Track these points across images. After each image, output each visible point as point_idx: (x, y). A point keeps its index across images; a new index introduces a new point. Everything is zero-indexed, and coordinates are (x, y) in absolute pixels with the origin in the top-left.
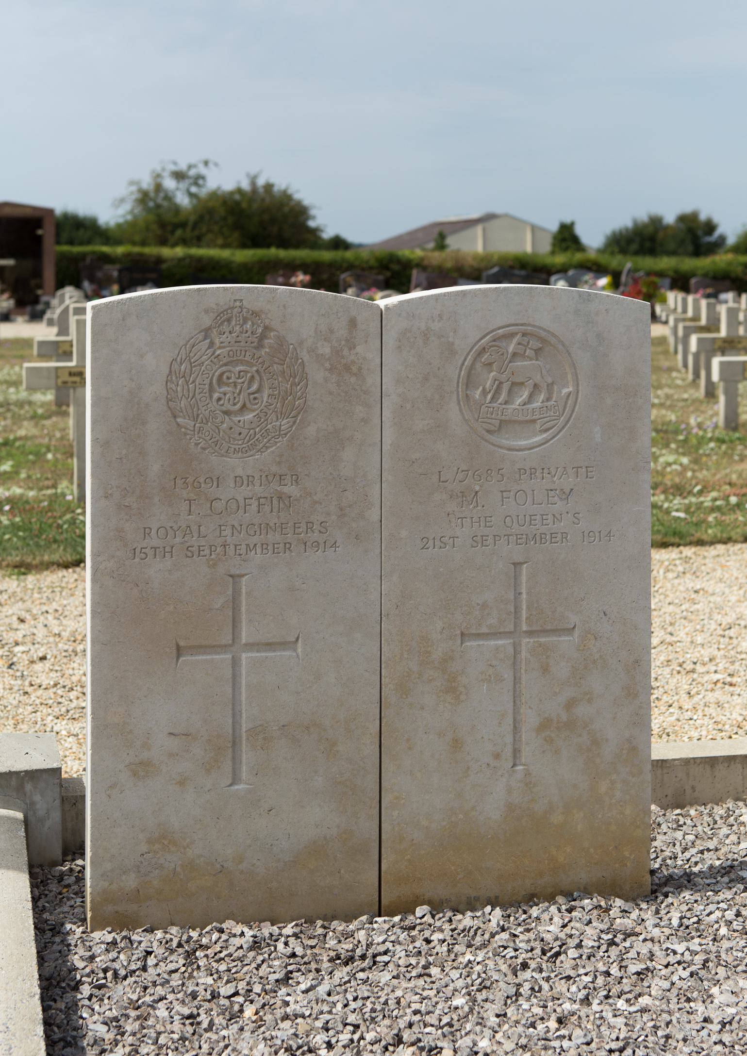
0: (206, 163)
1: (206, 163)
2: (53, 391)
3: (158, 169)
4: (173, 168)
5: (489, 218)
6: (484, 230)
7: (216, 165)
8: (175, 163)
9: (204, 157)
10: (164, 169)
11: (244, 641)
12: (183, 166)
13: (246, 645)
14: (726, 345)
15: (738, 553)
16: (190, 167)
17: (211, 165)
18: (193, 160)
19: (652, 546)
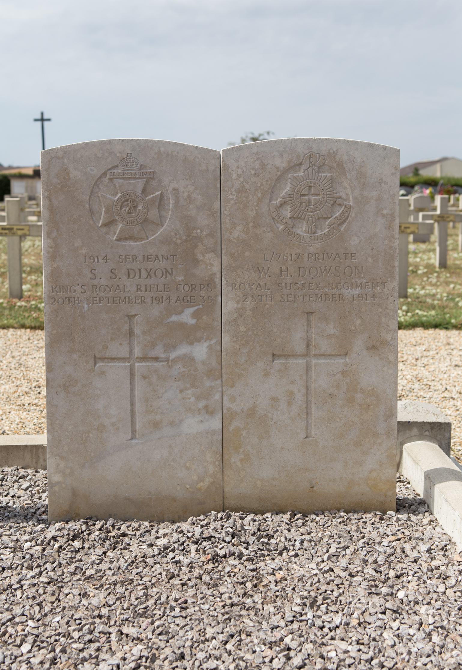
0: (268, 133)
1: (268, 133)
2: (408, 294)
3: (244, 137)
4: (251, 136)
5: (444, 159)
6: (441, 166)
7: (273, 133)
8: (253, 134)
9: (267, 130)
10: (247, 137)
11: (136, 356)
12: (256, 135)
13: (137, 358)
14: (440, 219)
15: (455, 336)
16: (260, 135)
17: (271, 134)
18: (262, 132)
19: (400, 328)
